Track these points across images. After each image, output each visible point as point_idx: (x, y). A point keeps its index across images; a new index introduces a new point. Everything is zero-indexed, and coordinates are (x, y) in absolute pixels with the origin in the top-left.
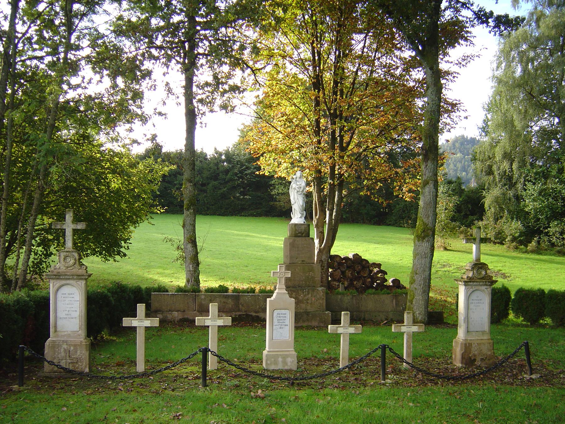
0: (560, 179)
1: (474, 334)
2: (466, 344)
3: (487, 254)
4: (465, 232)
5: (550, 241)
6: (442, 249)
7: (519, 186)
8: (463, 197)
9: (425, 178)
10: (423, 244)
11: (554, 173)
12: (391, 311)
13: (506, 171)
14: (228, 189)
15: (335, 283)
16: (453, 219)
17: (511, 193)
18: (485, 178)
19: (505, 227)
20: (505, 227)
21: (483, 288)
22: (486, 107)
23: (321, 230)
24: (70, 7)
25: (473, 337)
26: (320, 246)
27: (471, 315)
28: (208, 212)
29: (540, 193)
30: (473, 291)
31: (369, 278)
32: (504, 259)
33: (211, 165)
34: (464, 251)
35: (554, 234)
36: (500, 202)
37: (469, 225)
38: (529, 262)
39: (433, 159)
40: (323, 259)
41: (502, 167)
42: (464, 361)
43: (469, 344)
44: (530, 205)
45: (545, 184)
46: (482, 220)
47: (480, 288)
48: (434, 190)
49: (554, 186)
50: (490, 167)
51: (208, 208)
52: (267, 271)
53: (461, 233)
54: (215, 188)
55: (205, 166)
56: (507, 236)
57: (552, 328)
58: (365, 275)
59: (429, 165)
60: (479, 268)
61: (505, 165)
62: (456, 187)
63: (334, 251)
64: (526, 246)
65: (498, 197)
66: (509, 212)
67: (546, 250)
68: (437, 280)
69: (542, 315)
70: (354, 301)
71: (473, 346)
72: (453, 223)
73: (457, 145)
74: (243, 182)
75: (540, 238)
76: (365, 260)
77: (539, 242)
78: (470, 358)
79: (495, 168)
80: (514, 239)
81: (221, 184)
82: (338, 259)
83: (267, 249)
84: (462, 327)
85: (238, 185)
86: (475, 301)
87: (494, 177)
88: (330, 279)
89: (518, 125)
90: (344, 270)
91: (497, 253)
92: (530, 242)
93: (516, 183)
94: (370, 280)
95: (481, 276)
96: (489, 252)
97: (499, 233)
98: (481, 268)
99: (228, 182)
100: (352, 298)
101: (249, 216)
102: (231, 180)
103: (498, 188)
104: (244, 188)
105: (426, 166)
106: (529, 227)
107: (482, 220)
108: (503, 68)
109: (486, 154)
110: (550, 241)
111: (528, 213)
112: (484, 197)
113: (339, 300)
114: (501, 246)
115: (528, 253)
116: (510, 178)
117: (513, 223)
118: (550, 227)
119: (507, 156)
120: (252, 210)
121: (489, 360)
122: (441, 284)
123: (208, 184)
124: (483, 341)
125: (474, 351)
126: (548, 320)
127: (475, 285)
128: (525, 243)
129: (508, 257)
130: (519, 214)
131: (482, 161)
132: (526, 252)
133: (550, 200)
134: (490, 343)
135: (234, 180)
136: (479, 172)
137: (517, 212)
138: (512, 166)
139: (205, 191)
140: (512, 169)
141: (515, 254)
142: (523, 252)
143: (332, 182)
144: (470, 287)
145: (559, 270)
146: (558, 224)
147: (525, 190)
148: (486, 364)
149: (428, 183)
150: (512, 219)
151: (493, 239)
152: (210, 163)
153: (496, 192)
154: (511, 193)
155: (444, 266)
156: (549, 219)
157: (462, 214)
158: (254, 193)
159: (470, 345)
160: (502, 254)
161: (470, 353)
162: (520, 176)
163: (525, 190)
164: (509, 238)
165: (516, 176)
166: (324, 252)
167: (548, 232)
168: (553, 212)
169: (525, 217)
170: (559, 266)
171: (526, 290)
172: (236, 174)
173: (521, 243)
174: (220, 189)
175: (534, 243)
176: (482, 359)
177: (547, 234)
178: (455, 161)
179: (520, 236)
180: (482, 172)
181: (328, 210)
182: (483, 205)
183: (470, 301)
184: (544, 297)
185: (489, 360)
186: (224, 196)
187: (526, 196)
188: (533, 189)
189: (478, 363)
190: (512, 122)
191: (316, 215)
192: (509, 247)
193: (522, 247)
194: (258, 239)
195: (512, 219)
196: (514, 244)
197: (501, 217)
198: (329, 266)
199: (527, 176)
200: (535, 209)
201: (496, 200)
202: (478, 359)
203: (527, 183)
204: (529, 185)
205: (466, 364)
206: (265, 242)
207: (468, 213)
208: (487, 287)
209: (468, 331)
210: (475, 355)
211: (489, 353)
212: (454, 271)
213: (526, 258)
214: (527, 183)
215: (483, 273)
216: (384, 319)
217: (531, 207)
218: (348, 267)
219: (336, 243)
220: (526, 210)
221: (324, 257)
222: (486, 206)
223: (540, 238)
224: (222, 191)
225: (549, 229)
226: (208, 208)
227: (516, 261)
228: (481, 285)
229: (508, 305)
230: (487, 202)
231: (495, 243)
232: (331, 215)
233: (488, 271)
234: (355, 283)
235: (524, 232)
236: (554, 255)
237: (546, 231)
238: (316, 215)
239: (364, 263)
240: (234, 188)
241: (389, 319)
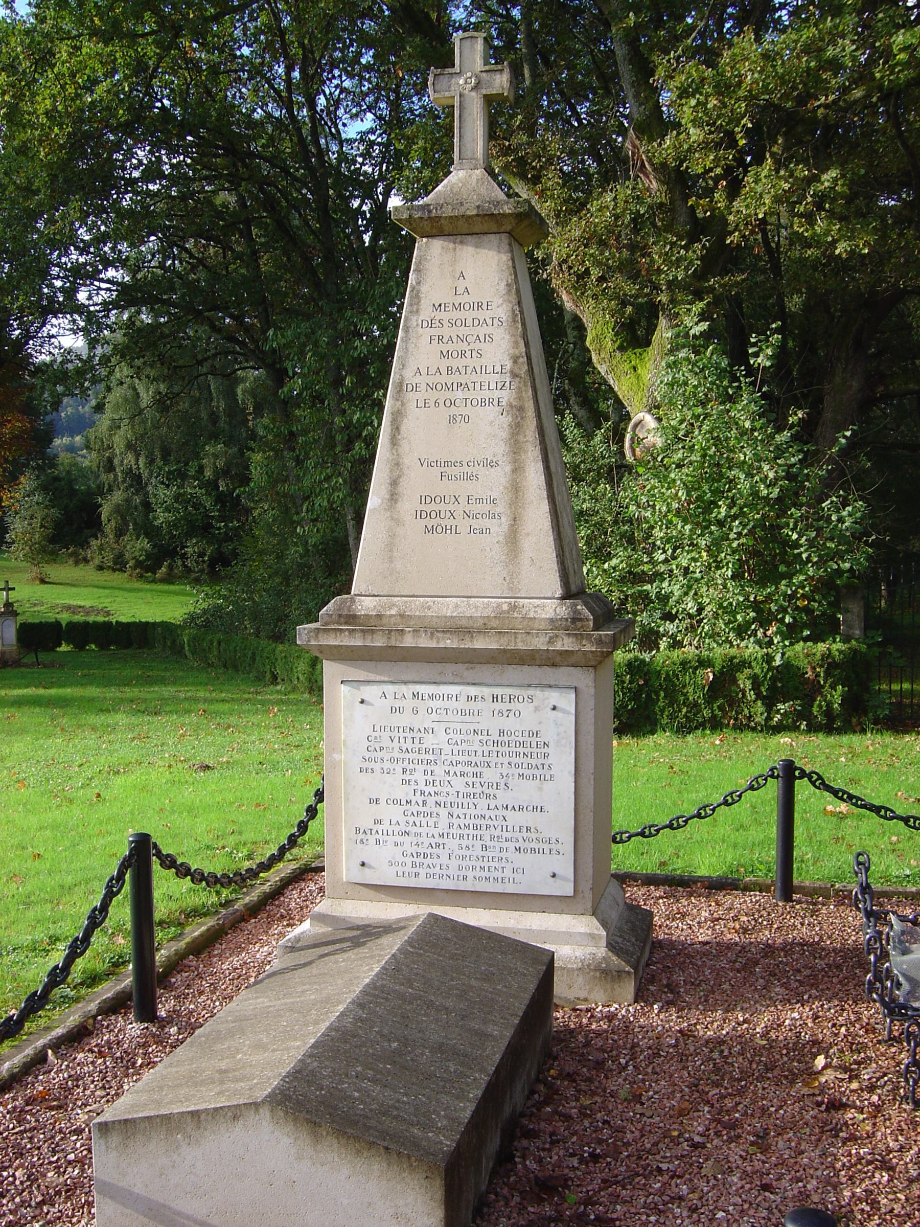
4: (75, 554)
11: (192, 472)
18: (103, 477)
24: (334, 515)
36: (121, 512)
37: (84, 544)
50: (110, 460)
53: (71, 555)
61: (130, 458)
65: (119, 505)
69: (87, 643)
79: (116, 461)
80: (139, 564)
91: (114, 584)
93: (146, 484)
96: (102, 583)
108: (558, 646)
111: (159, 528)
112: (101, 506)
116: (139, 477)
128: (153, 569)
130: (148, 530)
132: (154, 581)
141: (138, 585)
151: (111, 564)
153: (118, 496)
155: (35, 605)
156: (189, 535)
162: (151, 475)
164: (131, 563)
167: (185, 554)
200: (168, 523)
201: (117, 509)
217: (162, 520)
220: (156, 523)
230: (105, 512)
231: (114, 570)
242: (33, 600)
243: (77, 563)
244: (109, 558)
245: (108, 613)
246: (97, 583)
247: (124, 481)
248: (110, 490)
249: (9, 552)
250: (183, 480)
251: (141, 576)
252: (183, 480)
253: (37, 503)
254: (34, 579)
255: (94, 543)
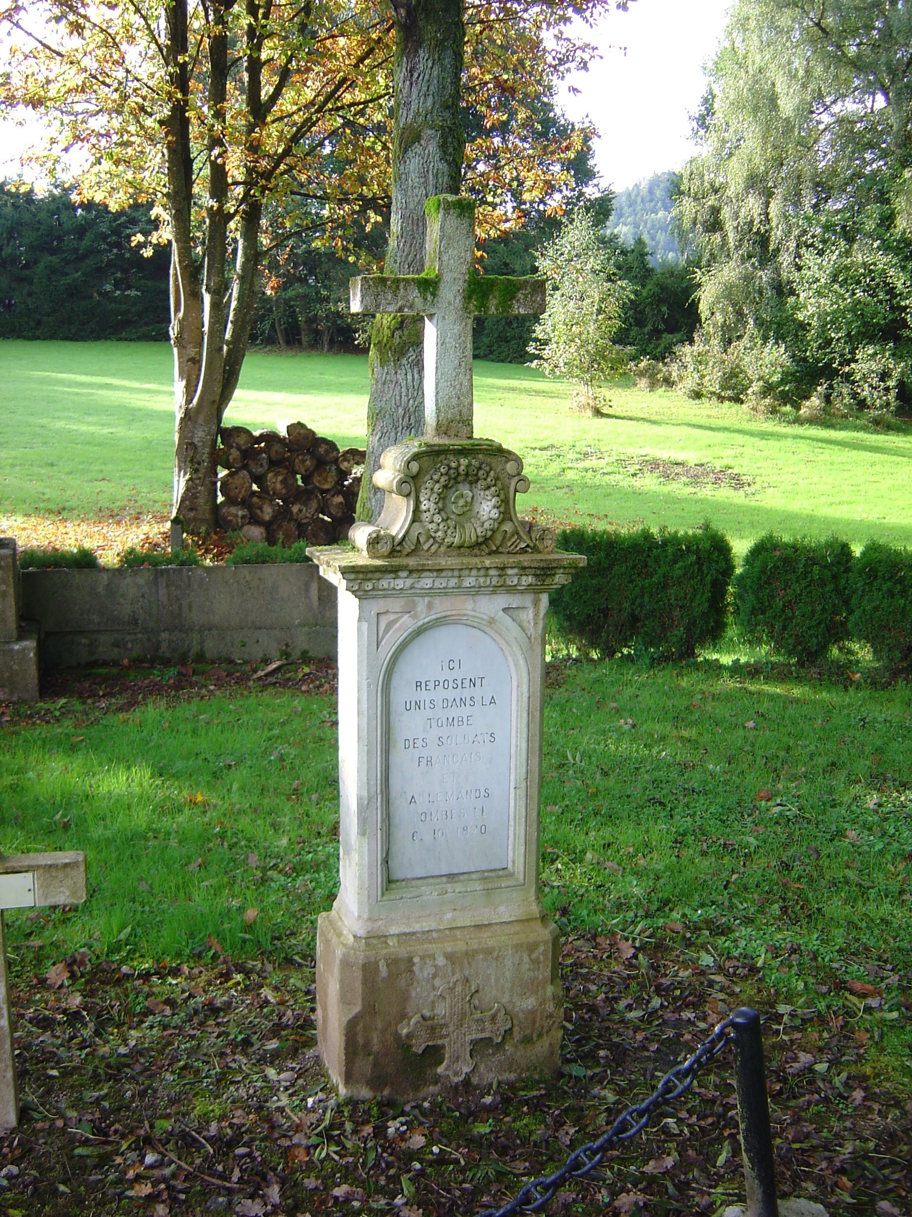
0: (883, 241)
1: (429, 893)
2: (369, 969)
3: (700, 427)
5: (854, 395)
6: (589, 413)
7: (785, 259)
8: (649, 287)
9: (405, 117)
10: (400, 377)
11: (870, 225)
12: (300, 625)
13: (752, 221)
14: (84, 274)
15: (233, 510)
16: (620, 338)
17: (764, 276)
18: (704, 238)
19: (747, 359)
20: (747, 359)
21: (491, 606)
22: (710, 65)
23: (192, 352)
25: (421, 917)
26: (189, 401)
27: (410, 777)
28: (38, 333)
29: (834, 278)
30: (419, 632)
31: (337, 493)
32: (739, 438)
33: (42, 215)
34: (643, 419)
35: (864, 378)
37: (663, 355)
38: (803, 446)
39: (440, 45)
40: (196, 440)
41: (743, 210)
42: (365, 1066)
43: (392, 962)
44: (810, 307)
45: (848, 253)
46: (692, 342)
47: (467, 606)
48: (443, 167)
49: (870, 260)
50: (715, 211)
51: (39, 323)
52: (101, 476)
53: (641, 374)
54: (53, 272)
55: (27, 217)
56: (752, 382)
57: (876, 682)
58: (326, 487)
59: (421, 67)
60: (454, 480)
61: (752, 205)
62: (631, 263)
63: (233, 415)
64: (797, 407)
66: (760, 323)
67: (845, 416)
68: (560, 493)
69: (837, 632)
70: (163, 591)
71: (422, 972)
72: (617, 347)
73: (658, 193)
74: (120, 256)
75: (831, 387)
76: (324, 441)
77: (827, 398)
78: (404, 1045)
79: (726, 213)
80: (768, 389)
81: (67, 262)
82: (242, 440)
83: (134, 416)
84: (355, 856)
85: (111, 264)
86: (440, 694)
87: (724, 238)
88: (220, 499)
89: (787, 106)
90: (260, 470)
92: (807, 398)
94: (339, 499)
95: (472, 532)
96: (704, 421)
97: (733, 375)
98: (471, 478)
99: (85, 256)
100: (156, 582)
101: (139, 339)
102: (92, 251)
103: (732, 264)
104: (125, 271)
105: (411, 72)
106: (805, 360)
107: (692, 342)
109: (706, 178)
110: (854, 395)
111: (803, 326)
113: (100, 590)
114: (736, 407)
115: (802, 424)
116: (763, 240)
117: (767, 350)
118: (856, 361)
119: (756, 183)
120: (146, 324)
121: (527, 1040)
122: (568, 504)
123: (36, 262)
124: (488, 940)
125: (431, 997)
126: (863, 653)
127: (430, 592)
129: (751, 434)
130: (783, 328)
131: (696, 199)
132: (798, 421)
133: (859, 294)
134: (531, 948)
135: (99, 251)
136: (687, 225)
137: (778, 324)
138: (767, 207)
139: (29, 281)
140: (767, 214)
141: (770, 426)
142: (789, 422)
143: (216, 205)
144: (396, 605)
145: (878, 468)
146: (875, 354)
147: (799, 268)
148: (510, 1065)
149: (417, 138)
150: (765, 339)
151: (716, 388)
152: (40, 209)
153: (729, 272)
154: (764, 276)
155: (586, 455)
157: (646, 330)
158: (150, 283)
159: (402, 967)
160: (738, 426)
161: (403, 1016)
163: (799, 268)
164: (756, 387)
165: (777, 234)
166: (200, 421)
168: (865, 324)
169: (796, 336)
170: (877, 456)
171: (786, 546)
172: (104, 237)
173: (785, 398)
174: (67, 274)
175: (815, 401)
176: (479, 1047)
177: (848, 377)
178: (653, 227)
179: (783, 382)
180: (695, 224)
181: (208, 290)
182: (695, 305)
183: (402, 693)
184: (848, 570)
185: (527, 1040)
186: (74, 292)
187: (801, 283)
188: (818, 267)
189: (455, 1068)
190: (773, 100)
191: (177, 309)
192: (754, 409)
193: (788, 408)
194: (126, 394)
195: (765, 339)
196: (768, 401)
197: (739, 338)
198: (217, 459)
199: (805, 232)
201: (728, 292)
202: (457, 1043)
203: (803, 251)
204: (809, 257)
205: (375, 1083)
206: (138, 401)
207: (661, 326)
208: (514, 601)
209: (389, 880)
210: (431, 1026)
211: (530, 1002)
212: (609, 469)
213: (795, 437)
214: (803, 251)
215: (487, 509)
216: (275, 653)
217: (811, 310)
218: (272, 463)
219: (239, 394)
220: (800, 316)
221: (200, 435)
222: (703, 308)
223: (831, 387)
224: (68, 280)
225: (853, 365)
226: (39, 323)
227: (772, 443)
228: (476, 592)
229: (723, 593)
230: (707, 295)
231: (721, 399)
232: (219, 307)
233: (523, 504)
234: (295, 509)
235: (793, 374)
236: (864, 429)
237: (847, 369)
238: (177, 309)
239: (322, 450)
240: (100, 272)
241: (296, 654)
242: (581, 447)
243: (653, 386)
244: (713, 380)
245: (738, 482)
246: (694, 421)
247: (737, 248)
248: (736, 247)
249: (539, 357)
250: (851, 240)
251: (774, 411)
252: (851, 240)
253: (594, 271)
254: (582, 408)
255: (687, 351)
